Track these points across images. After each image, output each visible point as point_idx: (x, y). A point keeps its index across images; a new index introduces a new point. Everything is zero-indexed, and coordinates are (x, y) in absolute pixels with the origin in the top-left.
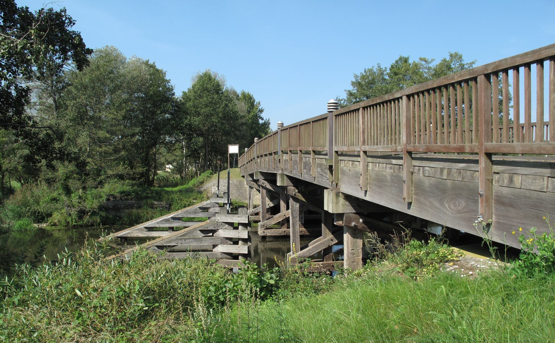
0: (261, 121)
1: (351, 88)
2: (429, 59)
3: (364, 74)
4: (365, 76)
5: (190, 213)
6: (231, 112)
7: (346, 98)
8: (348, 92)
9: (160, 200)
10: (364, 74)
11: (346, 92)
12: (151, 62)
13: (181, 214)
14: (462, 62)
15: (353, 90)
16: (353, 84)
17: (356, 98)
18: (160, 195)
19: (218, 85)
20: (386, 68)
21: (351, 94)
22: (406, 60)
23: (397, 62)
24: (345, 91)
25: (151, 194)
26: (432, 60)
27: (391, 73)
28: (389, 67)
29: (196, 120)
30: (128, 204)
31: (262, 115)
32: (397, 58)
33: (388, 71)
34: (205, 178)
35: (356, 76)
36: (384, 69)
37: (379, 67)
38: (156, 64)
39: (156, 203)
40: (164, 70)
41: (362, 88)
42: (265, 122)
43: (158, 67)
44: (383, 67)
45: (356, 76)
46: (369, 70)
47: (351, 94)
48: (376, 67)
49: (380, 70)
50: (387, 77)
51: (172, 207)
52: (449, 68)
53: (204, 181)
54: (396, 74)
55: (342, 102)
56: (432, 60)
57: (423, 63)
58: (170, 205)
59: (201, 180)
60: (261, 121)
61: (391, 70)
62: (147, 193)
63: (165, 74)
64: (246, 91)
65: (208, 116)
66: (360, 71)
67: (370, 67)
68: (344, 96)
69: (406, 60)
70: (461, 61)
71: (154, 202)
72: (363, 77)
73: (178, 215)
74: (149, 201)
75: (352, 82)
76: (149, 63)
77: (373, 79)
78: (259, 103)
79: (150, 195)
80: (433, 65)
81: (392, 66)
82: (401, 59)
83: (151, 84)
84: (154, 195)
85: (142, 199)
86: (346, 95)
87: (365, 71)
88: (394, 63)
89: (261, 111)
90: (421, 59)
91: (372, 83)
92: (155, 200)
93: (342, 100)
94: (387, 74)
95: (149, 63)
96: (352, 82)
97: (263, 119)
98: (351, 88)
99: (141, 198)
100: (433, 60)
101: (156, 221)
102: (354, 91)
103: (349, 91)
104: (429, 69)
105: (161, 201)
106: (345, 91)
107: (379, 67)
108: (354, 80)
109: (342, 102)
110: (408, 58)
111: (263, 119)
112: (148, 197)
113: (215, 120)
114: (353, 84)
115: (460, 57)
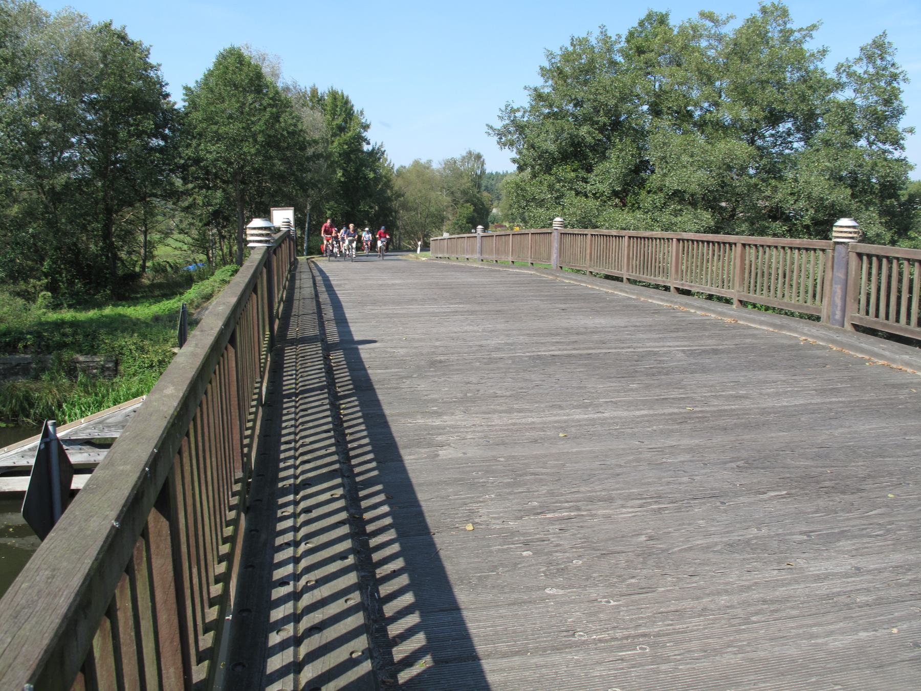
0: (366, 148)
1: (538, 82)
2: (721, 12)
3: (571, 49)
4: (572, 54)
5: (109, 427)
6: (285, 133)
7: (527, 106)
8: (532, 92)
9: (92, 350)
10: (571, 49)
11: (527, 92)
12: (116, 26)
13: (85, 428)
14: (788, 26)
15: (543, 87)
16: (544, 72)
17: (551, 106)
18: (93, 339)
19: (259, 76)
20: (619, 36)
21: (539, 96)
22: (662, 20)
23: (641, 24)
24: (525, 88)
25: (73, 335)
26: (730, 18)
27: (631, 49)
28: (625, 34)
29: (212, 151)
30: (14, 363)
31: (367, 134)
32: (643, 16)
33: (623, 44)
34: (217, 285)
35: (550, 55)
36: (613, 39)
37: (604, 33)
38: (128, 31)
39: (82, 358)
40: (146, 44)
41: (565, 81)
42: (373, 149)
43: (132, 36)
44: (612, 34)
45: (550, 55)
46: (580, 41)
47: (539, 96)
48: (596, 33)
49: (606, 43)
50: (619, 58)
51: (121, 368)
52: (764, 38)
53: (213, 292)
54: (640, 51)
55: (518, 114)
56: (730, 18)
57: (709, 24)
58: (117, 363)
59: (208, 290)
60: (366, 148)
61: (628, 41)
62: (64, 335)
63: (148, 50)
64: (338, 88)
65: (235, 142)
66: (559, 43)
67: (583, 35)
68: (524, 101)
69: (662, 20)
70: (785, 23)
71: (78, 356)
72: (567, 57)
73: (76, 433)
74: (66, 355)
75: (542, 69)
76: (113, 28)
77: (592, 61)
78: (362, 113)
79: (69, 340)
80: (729, 30)
81: (631, 34)
82: (649, 17)
83: (102, 70)
84: (80, 338)
85: (48, 349)
86: (528, 99)
87: (572, 44)
88: (636, 25)
89: (366, 127)
90: (703, 15)
91: (589, 70)
92: (81, 352)
93: (518, 110)
94: (621, 51)
95: (113, 28)
96: (542, 69)
97: (368, 143)
98: (538, 82)
99: (48, 346)
100: (732, 17)
101: (19, 450)
102: (547, 90)
103: (536, 90)
104: (720, 38)
105: (95, 354)
106: (525, 88)
107: (604, 33)
108: (547, 65)
109: (518, 114)
110: (667, 15)
111: (368, 143)
112: (64, 345)
113: (249, 148)
114: (544, 72)
115: (785, 13)
